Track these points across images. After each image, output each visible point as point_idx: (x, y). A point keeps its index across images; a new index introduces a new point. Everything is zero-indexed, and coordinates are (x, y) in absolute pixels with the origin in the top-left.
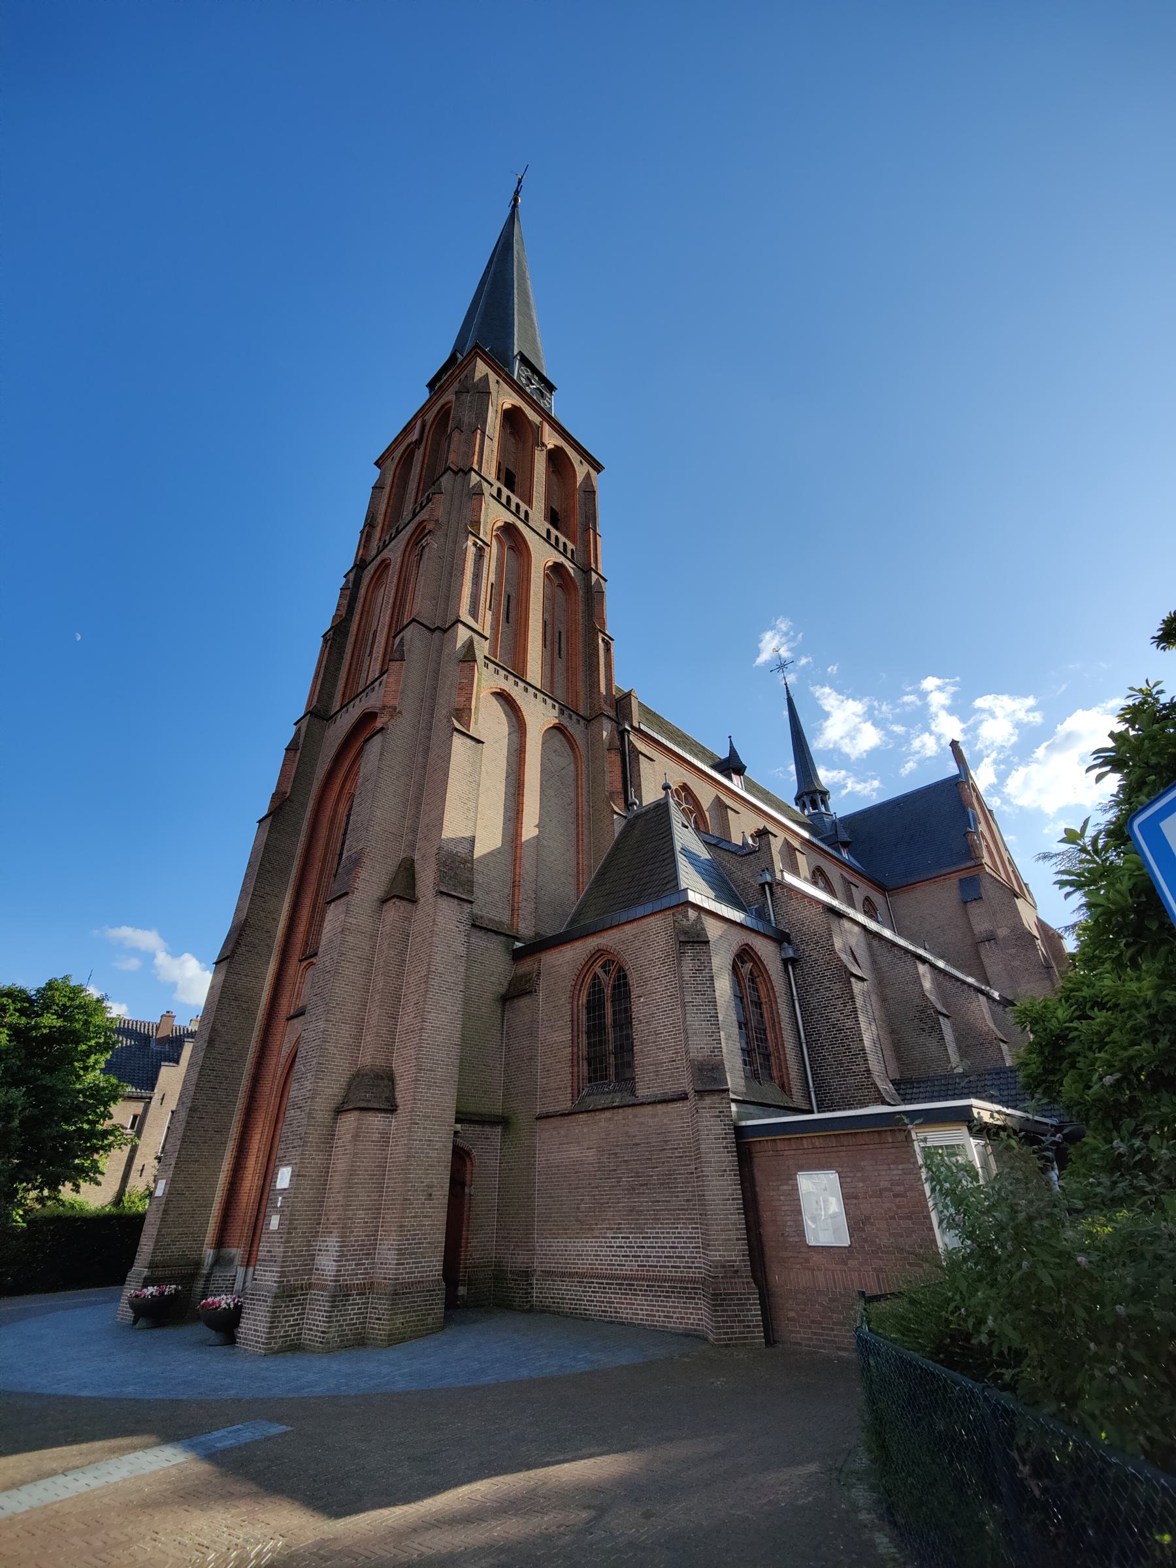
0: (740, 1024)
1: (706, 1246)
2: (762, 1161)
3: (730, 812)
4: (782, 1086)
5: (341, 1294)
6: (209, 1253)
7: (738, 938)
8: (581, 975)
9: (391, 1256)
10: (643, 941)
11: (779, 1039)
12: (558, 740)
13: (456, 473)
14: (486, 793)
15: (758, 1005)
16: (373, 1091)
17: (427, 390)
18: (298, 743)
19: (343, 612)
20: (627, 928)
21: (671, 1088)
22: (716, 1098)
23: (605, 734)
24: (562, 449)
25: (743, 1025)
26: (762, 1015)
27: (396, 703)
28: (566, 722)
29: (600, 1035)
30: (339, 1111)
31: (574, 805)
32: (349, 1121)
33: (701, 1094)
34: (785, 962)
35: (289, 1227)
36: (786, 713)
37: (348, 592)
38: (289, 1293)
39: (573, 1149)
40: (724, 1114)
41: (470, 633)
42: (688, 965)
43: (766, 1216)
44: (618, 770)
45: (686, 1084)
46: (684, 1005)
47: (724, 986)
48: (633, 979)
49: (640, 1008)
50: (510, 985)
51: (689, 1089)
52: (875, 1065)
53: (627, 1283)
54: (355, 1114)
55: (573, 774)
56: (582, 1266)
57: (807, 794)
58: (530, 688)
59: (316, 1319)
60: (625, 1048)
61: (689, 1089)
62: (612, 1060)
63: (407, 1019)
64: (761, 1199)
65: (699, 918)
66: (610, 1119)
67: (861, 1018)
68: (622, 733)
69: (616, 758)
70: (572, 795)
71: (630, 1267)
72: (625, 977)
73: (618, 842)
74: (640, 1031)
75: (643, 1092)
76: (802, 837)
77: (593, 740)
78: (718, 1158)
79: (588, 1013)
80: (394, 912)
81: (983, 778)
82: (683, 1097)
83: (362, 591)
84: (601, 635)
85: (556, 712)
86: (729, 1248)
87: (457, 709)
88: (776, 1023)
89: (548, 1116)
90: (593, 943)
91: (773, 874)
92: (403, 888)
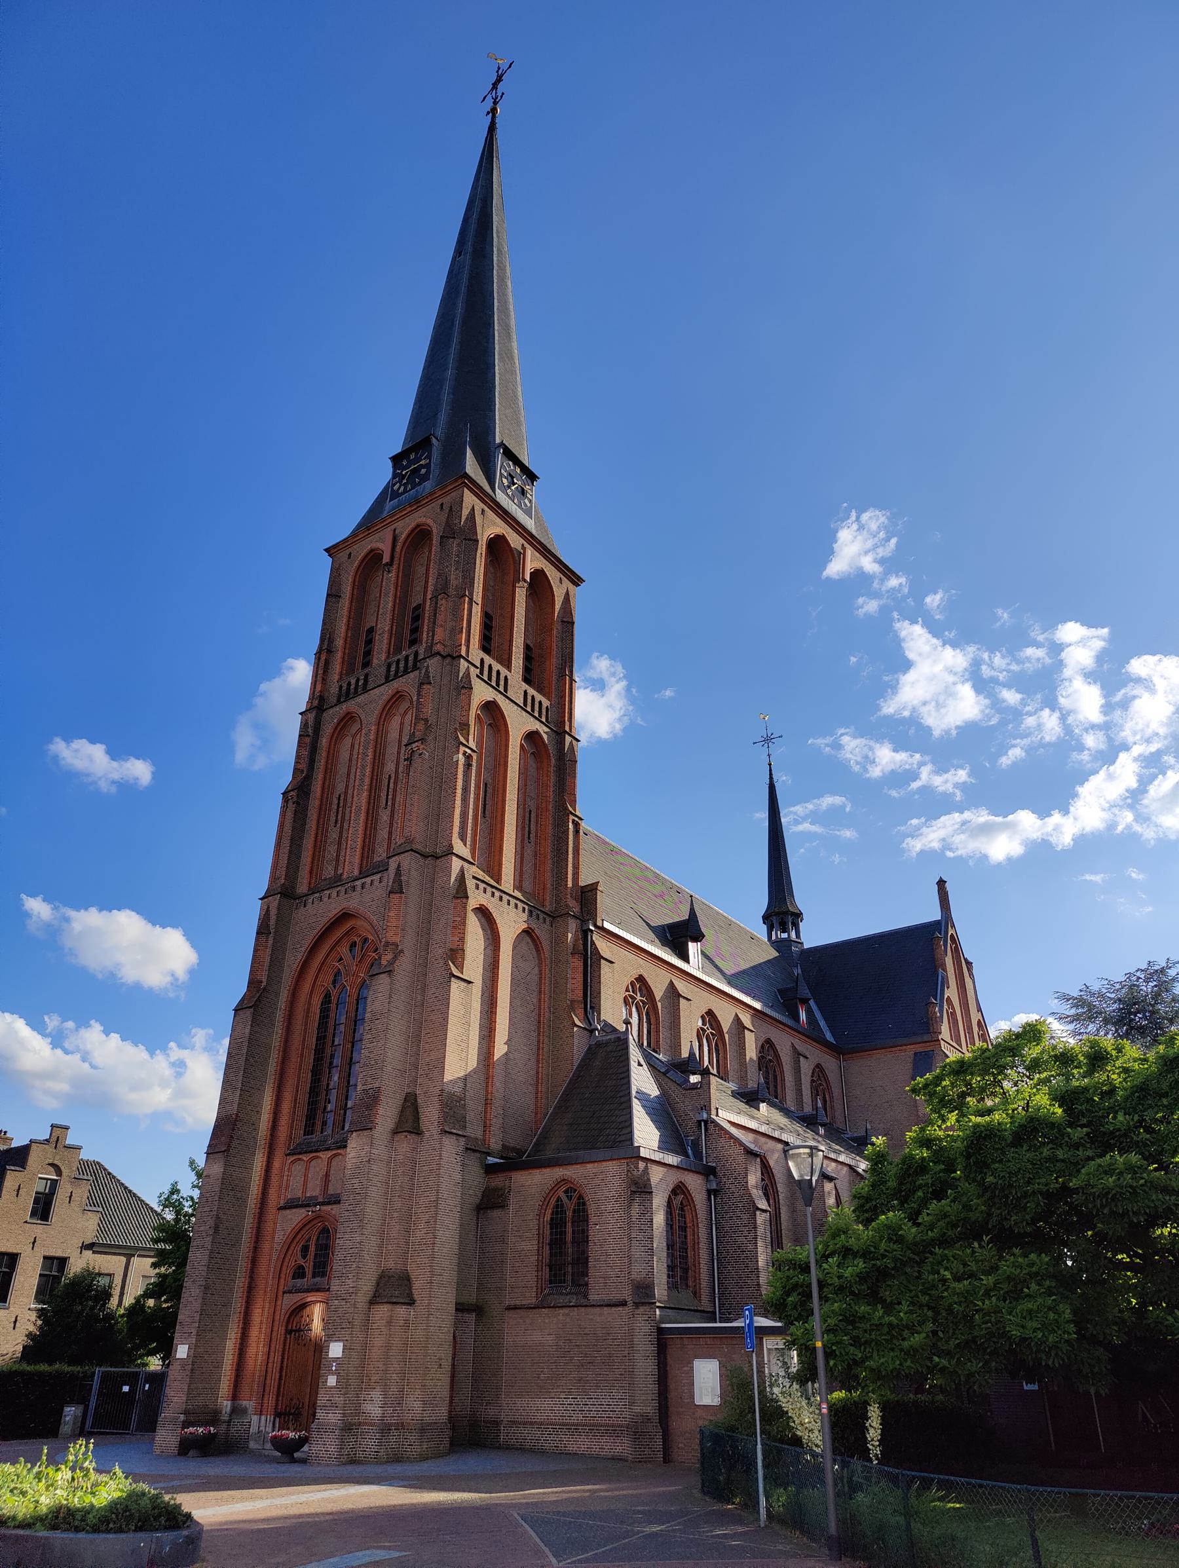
0: (668, 1246)
1: (632, 1403)
2: (673, 1352)
3: (682, 1001)
4: (695, 1294)
5: (385, 1429)
6: (226, 1405)
7: (674, 1178)
8: (547, 1198)
9: (417, 1406)
10: (601, 1180)
11: (697, 1255)
12: (527, 947)
13: (444, 657)
14: (472, 1032)
15: (683, 1229)
16: (394, 1288)
17: (390, 464)
18: (268, 926)
19: (304, 766)
20: (589, 1166)
21: (616, 1296)
22: (647, 1308)
23: (570, 935)
24: (543, 571)
25: (670, 1246)
26: (686, 1237)
27: (397, 939)
28: (533, 926)
29: (561, 1248)
30: (373, 1302)
31: (536, 1011)
32: (382, 1311)
33: (637, 1305)
34: (709, 1192)
35: (343, 1385)
36: (763, 816)
37: (308, 740)
38: (348, 1428)
39: (537, 1333)
40: (651, 1318)
41: (461, 862)
42: (636, 1209)
43: (672, 1386)
44: (579, 977)
45: (626, 1294)
46: (630, 1239)
47: (659, 1219)
48: (592, 1209)
49: (595, 1233)
50: (483, 1196)
51: (629, 1299)
52: (763, 1279)
53: (574, 1428)
54: (389, 1306)
55: (536, 978)
56: (541, 1417)
57: (777, 914)
58: (504, 896)
59: (370, 1443)
60: (582, 1261)
61: (629, 1299)
62: (570, 1269)
63: (420, 1233)
64: (670, 1376)
65: (646, 1168)
66: (568, 1315)
67: (760, 1243)
68: (586, 932)
69: (579, 964)
70: (535, 1000)
71: (577, 1418)
72: (584, 1204)
73: (581, 1067)
74: (594, 1251)
75: (594, 1297)
76: (755, 1009)
77: (558, 941)
78: (645, 1347)
79: (551, 1228)
80: (404, 1145)
81: (965, 929)
82: (623, 1304)
83: (324, 741)
84: (571, 817)
85: (525, 916)
86: (646, 1404)
87: (451, 950)
88: (696, 1243)
89: (515, 1308)
90: (559, 1172)
91: (709, 1114)
92: (409, 1121)
